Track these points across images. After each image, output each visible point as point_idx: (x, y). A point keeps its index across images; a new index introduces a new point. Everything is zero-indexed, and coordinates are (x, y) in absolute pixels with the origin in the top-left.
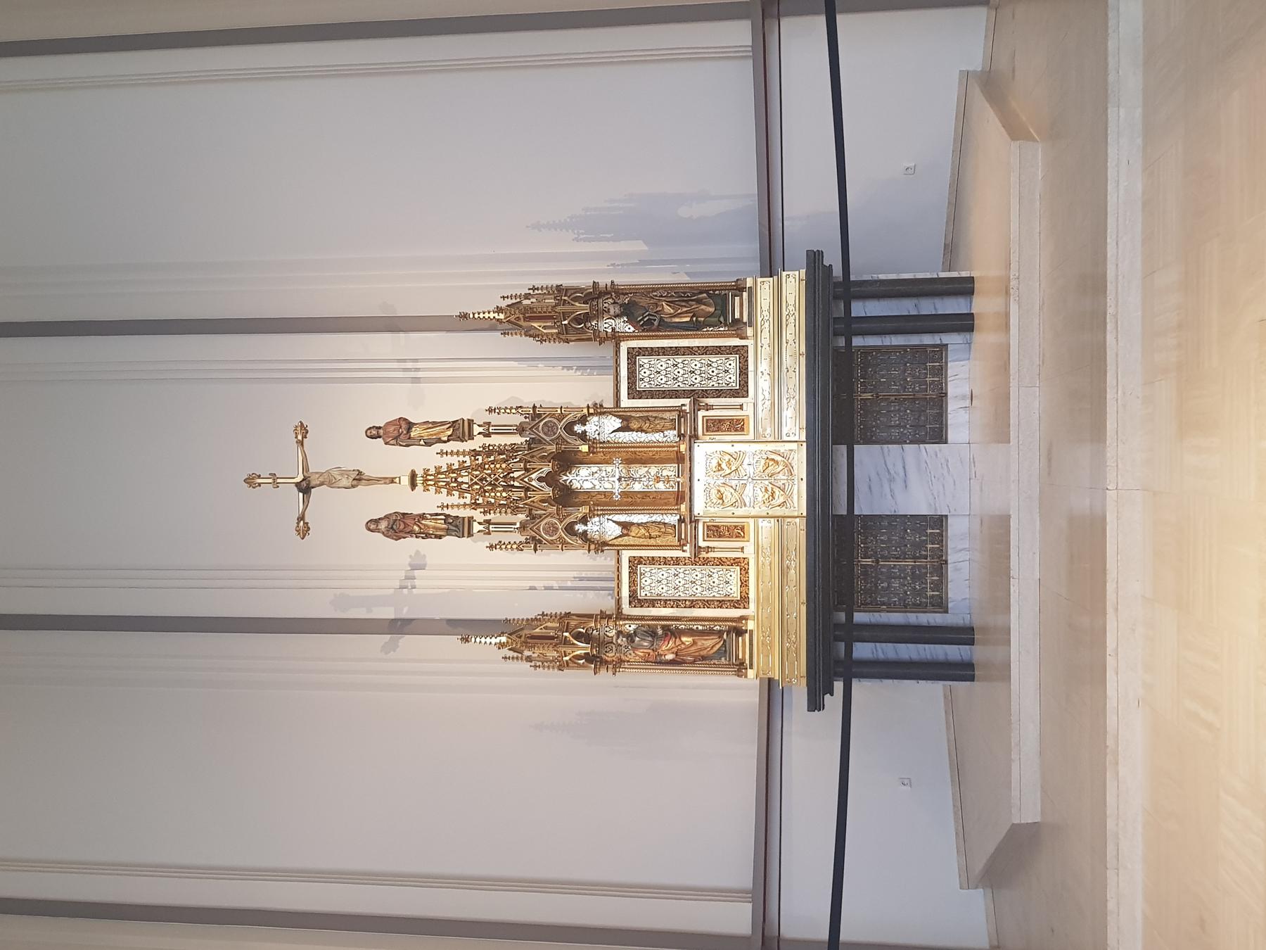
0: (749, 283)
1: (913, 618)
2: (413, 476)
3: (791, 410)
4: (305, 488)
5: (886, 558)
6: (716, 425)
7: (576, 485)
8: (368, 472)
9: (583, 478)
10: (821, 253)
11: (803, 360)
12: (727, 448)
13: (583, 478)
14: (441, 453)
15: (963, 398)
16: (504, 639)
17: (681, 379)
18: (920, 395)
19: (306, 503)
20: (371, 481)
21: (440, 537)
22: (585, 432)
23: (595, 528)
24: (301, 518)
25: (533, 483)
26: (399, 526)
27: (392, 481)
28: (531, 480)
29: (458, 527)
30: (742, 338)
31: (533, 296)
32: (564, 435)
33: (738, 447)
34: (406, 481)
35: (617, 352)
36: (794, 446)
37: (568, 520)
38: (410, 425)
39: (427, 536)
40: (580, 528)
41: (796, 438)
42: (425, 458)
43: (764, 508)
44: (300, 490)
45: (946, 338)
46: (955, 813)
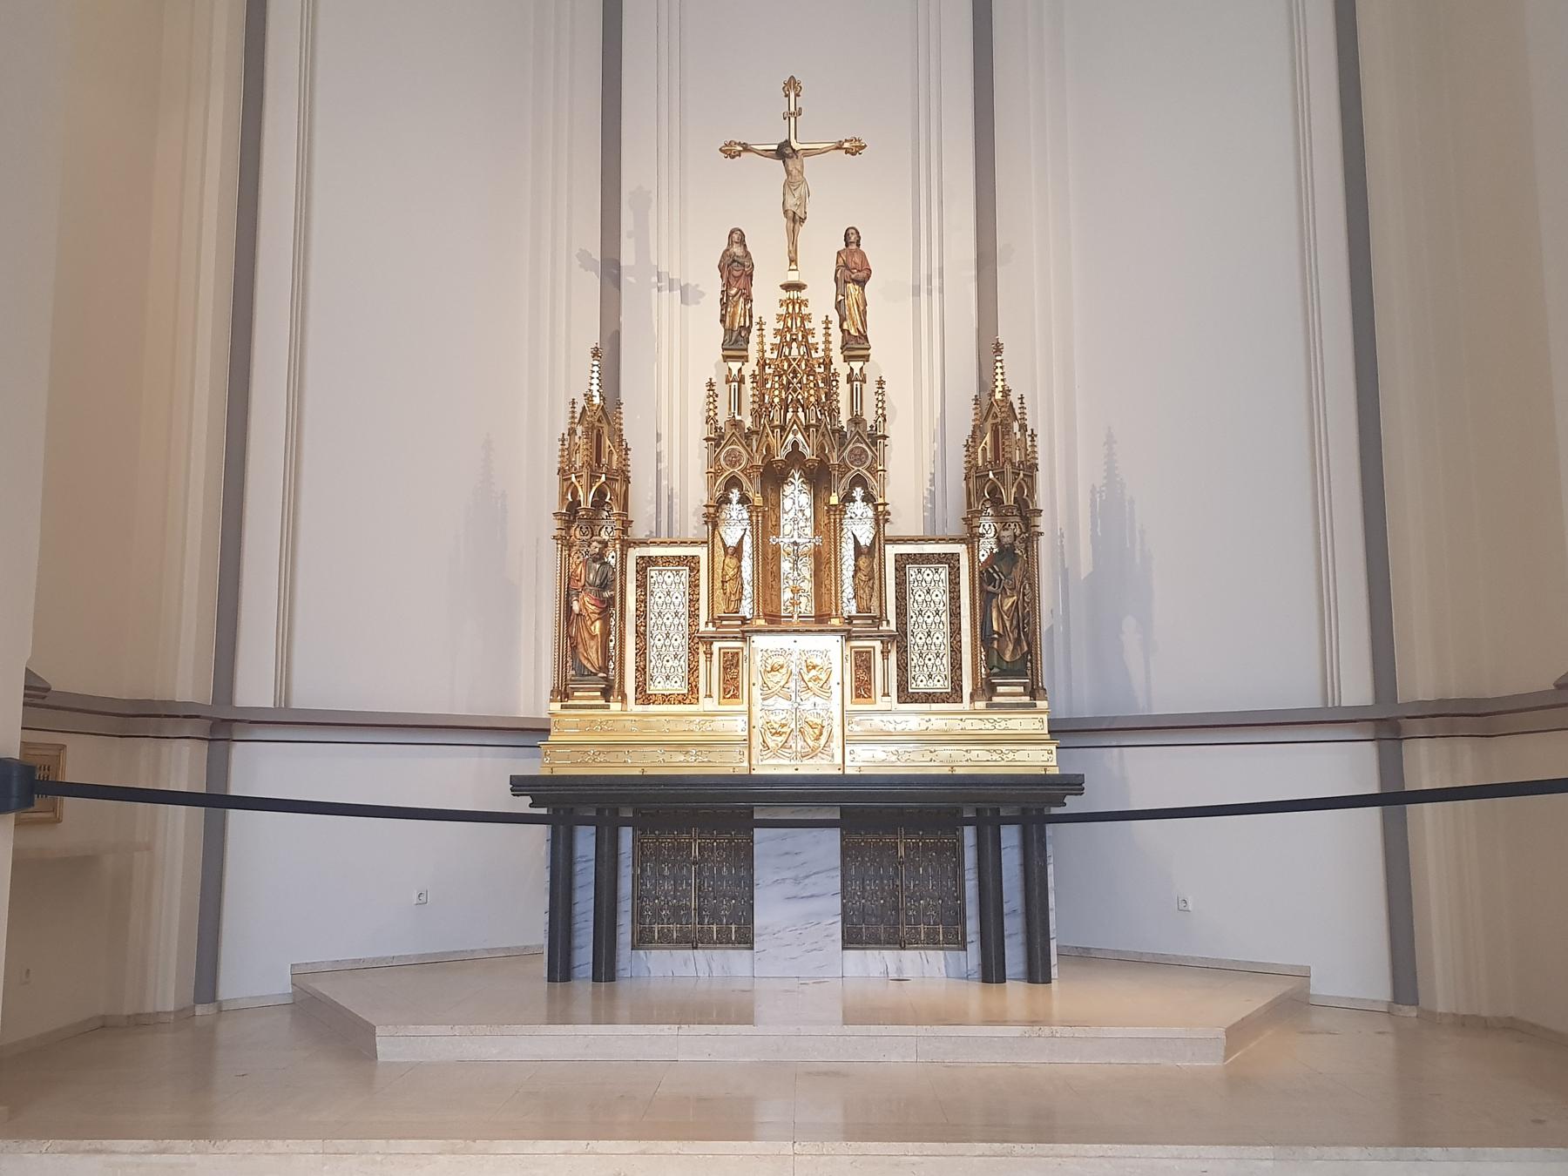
0: (1042, 704)
1: (625, 907)
2: (799, 287)
3: (883, 756)
4: (783, 152)
5: (699, 874)
6: (863, 663)
7: (788, 489)
9: (796, 498)
12: (836, 677)
13: (796, 498)
14: (827, 322)
15: (899, 970)
16: (597, 400)
17: (920, 620)
19: (765, 153)
20: (793, 242)
21: (723, 321)
23: (734, 514)
24: (746, 148)
25: (791, 436)
26: (736, 270)
27: (793, 261)
29: (735, 343)
30: (972, 696)
31: (1024, 435)
32: (850, 475)
33: (837, 690)
34: (793, 277)
35: (953, 540)
36: (838, 760)
37: (744, 479)
38: (862, 283)
40: (735, 495)
42: (821, 303)
43: (761, 722)
45: (974, 949)
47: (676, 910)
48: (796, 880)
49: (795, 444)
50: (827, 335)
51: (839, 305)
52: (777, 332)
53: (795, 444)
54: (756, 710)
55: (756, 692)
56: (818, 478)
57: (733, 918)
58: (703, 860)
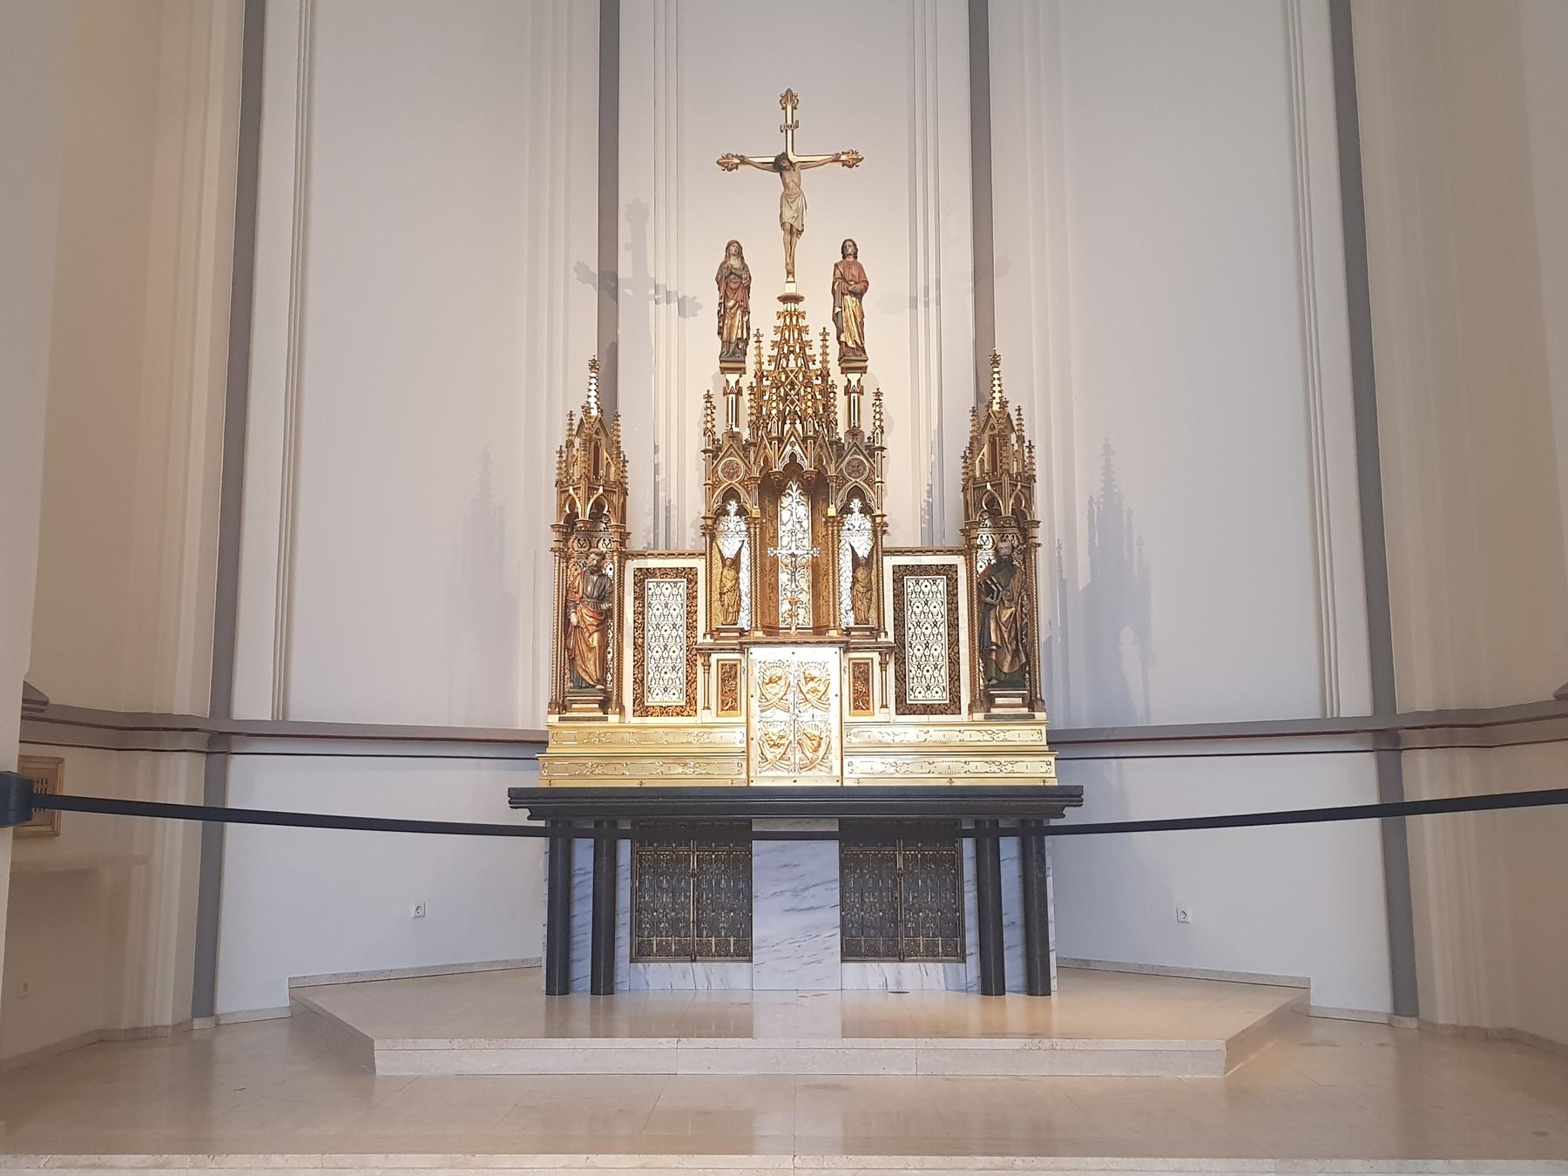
0: (1040, 716)
1: (624, 919)
2: (796, 299)
3: (882, 768)
4: (780, 165)
5: (697, 886)
6: (861, 674)
7: (786, 501)
8: (800, 243)
9: (794, 509)
12: (834, 689)
13: (794, 509)
14: (825, 334)
15: (899, 983)
16: (594, 412)
17: (918, 631)
19: (762, 166)
21: (720, 333)
23: (732, 526)
24: (743, 161)
25: (789, 448)
26: (734, 282)
27: (790, 273)
28: (793, 445)
29: (732, 356)
30: (970, 707)
32: (848, 486)
33: (835, 702)
34: (790, 289)
35: (951, 552)
36: (837, 772)
37: (742, 492)
38: (859, 295)
39: (722, 317)
40: (732, 507)
42: (818, 314)
43: (759, 734)
44: (778, 159)
45: (973, 961)
48: (795, 893)
49: (793, 456)
51: (836, 317)
52: (775, 344)
53: (793, 456)
54: (754, 721)
55: (755, 704)
57: (732, 930)
58: (702, 872)
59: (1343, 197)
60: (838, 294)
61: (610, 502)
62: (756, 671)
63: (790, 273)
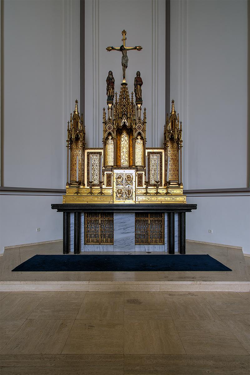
0: (181, 187)
1: (82, 235)
2: (126, 84)
3: (145, 199)
4: (122, 49)
5: (101, 227)
6: (140, 177)
7: (123, 136)
8: (127, 70)
9: (125, 140)
10: (196, 209)
11: (160, 202)
12: (134, 180)
13: (125, 140)
14: (132, 93)
15: (148, 250)
16: (76, 113)
17: (153, 167)
18: (149, 237)
19: (118, 50)
20: (124, 71)
21: (107, 94)
22: (138, 139)
23: (110, 142)
24: (113, 49)
25: (123, 120)
26: (110, 81)
27: (124, 78)
28: (124, 119)
29: (110, 99)
30: (164, 185)
31: (178, 123)
32: (137, 132)
33: (134, 183)
34: (124, 82)
35: (161, 149)
36: (134, 200)
37: (112, 133)
38: (141, 85)
39: (108, 90)
40: (110, 138)
41: (136, 200)
42: (131, 89)
43: (116, 191)
44: (121, 47)
45: (166, 245)
46: (29, 244)
47: (95, 235)
48: (124, 229)
49: (124, 123)
50: (132, 97)
51: (135, 90)
52: (120, 96)
53: (124, 123)
54: (115, 188)
55: (115, 183)
56: (130, 132)
57: (109, 237)
58: (102, 224)
59: (62, 271)
60: (136, 85)
61: (80, 135)
62: (115, 175)
63: (124, 78)
